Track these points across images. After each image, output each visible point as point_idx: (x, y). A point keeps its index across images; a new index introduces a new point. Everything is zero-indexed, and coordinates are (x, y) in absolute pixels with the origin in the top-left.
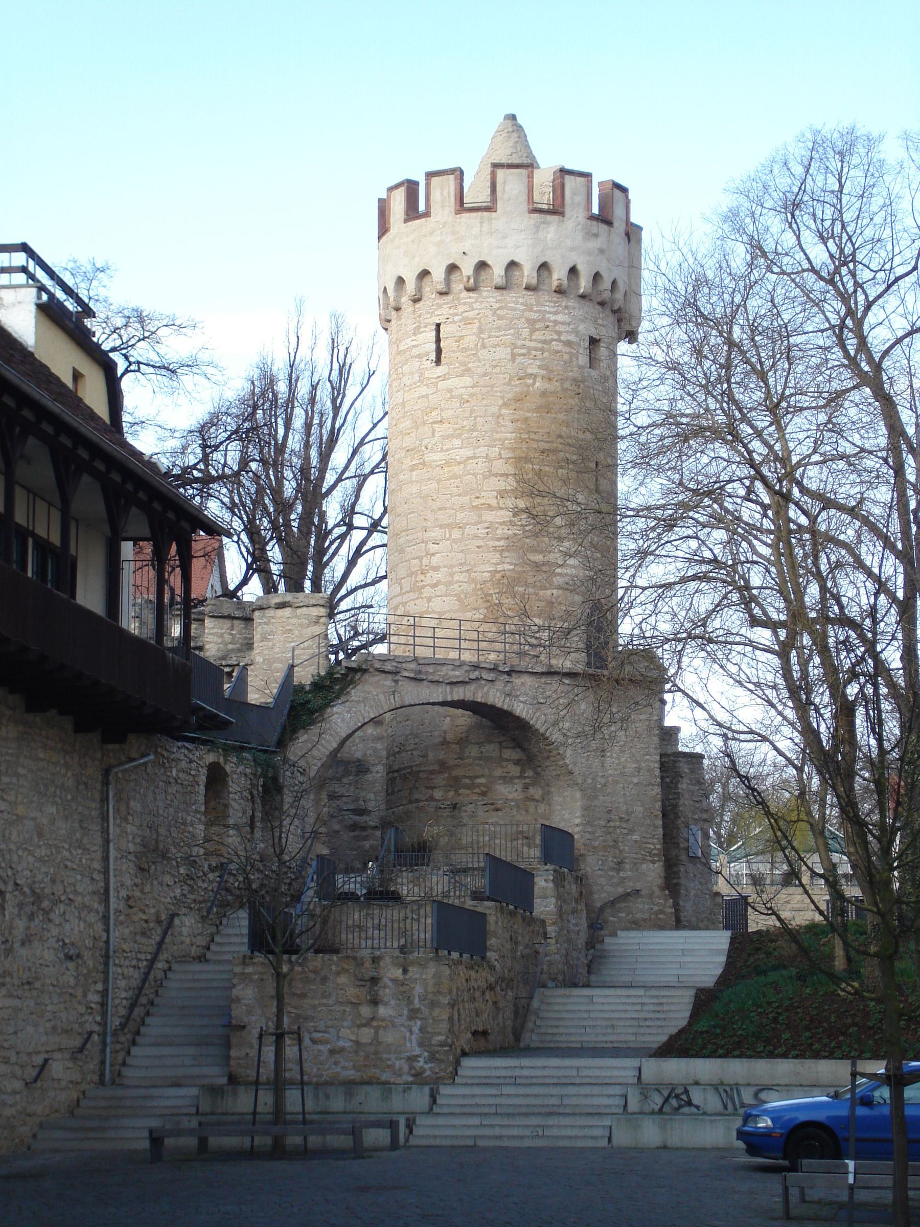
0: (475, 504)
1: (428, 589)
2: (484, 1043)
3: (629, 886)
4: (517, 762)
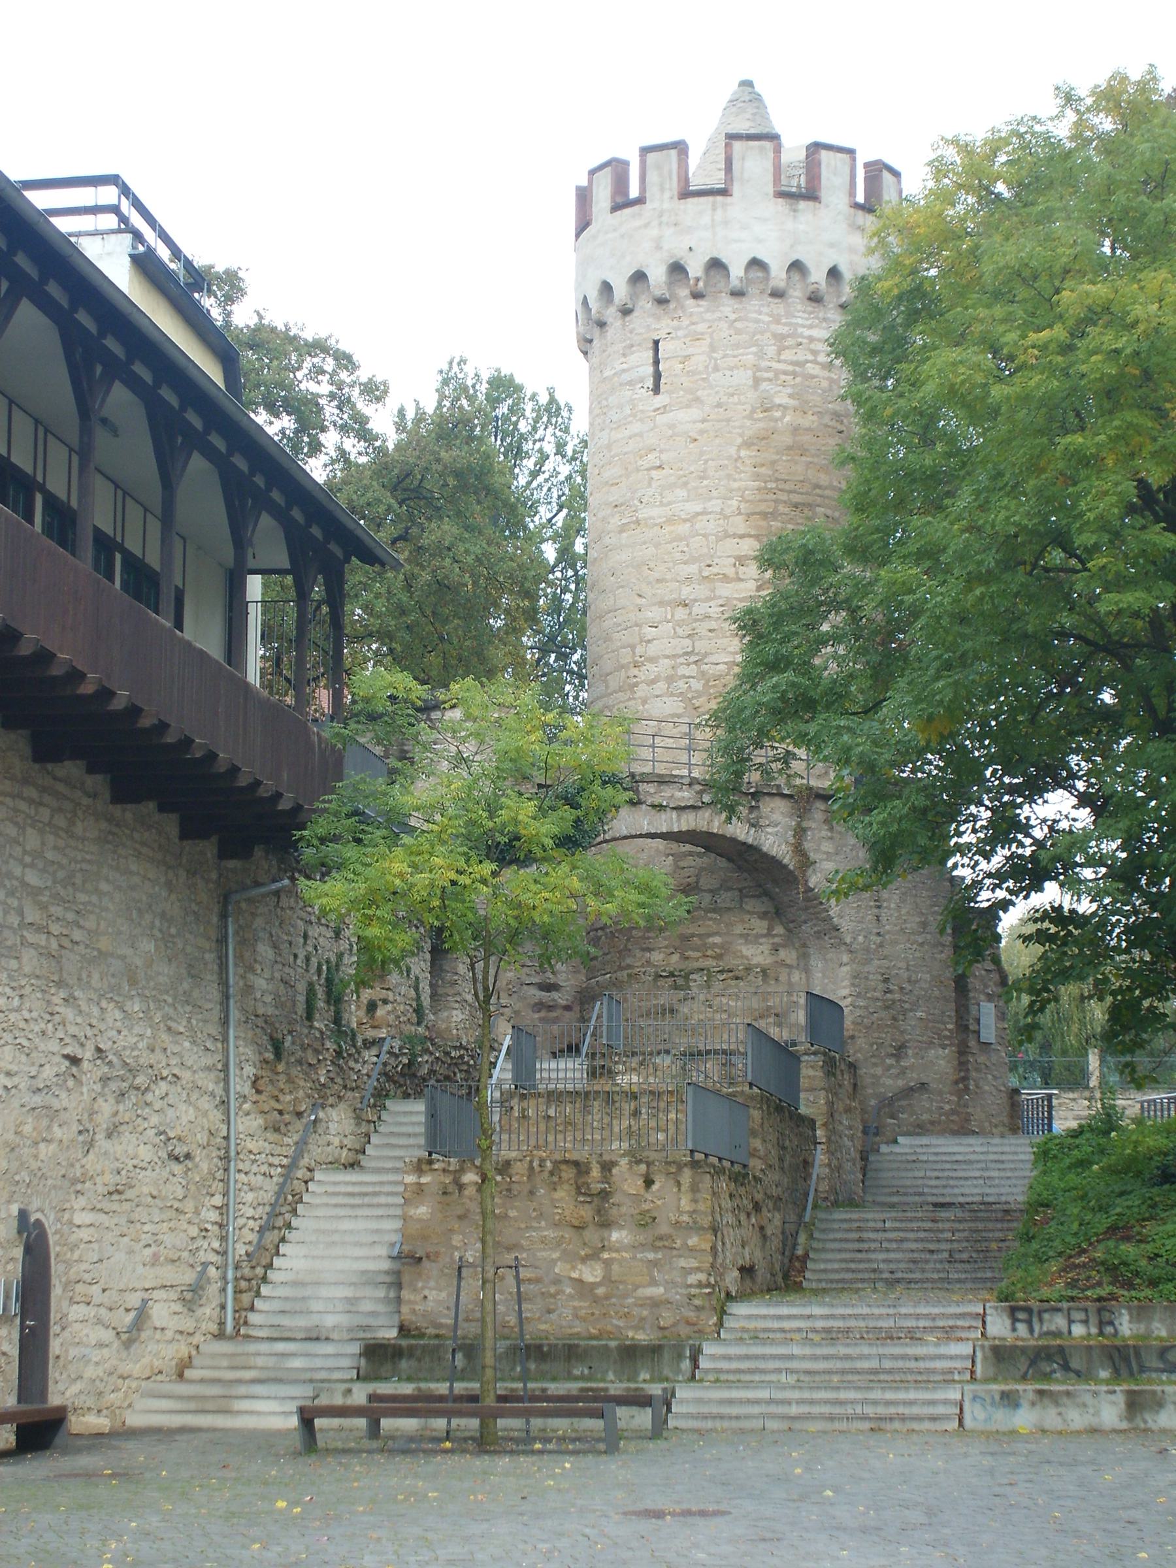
0: (705, 574)
1: (643, 686)
2: (754, 1281)
3: (913, 1078)
4: (764, 916)
